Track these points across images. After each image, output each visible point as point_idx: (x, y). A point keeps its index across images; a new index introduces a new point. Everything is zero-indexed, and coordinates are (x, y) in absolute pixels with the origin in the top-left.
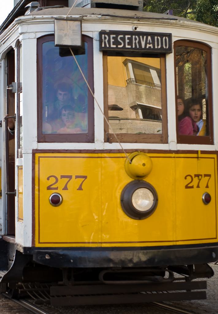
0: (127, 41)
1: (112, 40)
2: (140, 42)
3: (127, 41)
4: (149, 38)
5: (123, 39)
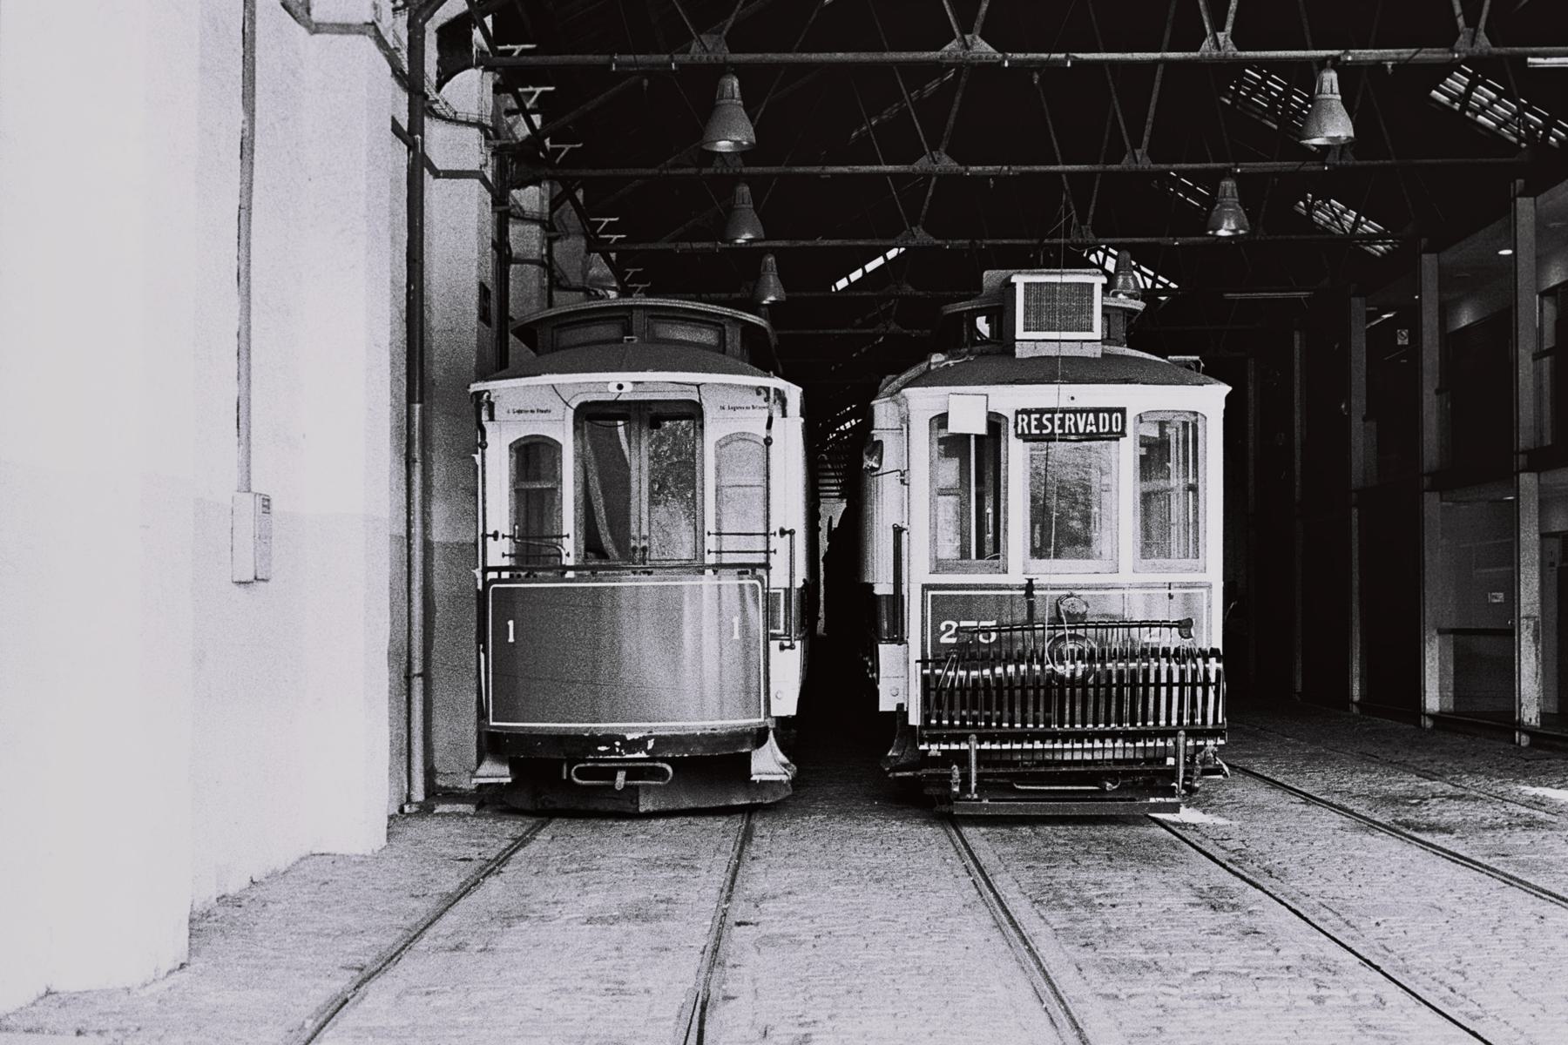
0: (1057, 422)
1: (1034, 423)
2: (1076, 424)
3: (1057, 422)
4: (1091, 416)
5: (1051, 420)
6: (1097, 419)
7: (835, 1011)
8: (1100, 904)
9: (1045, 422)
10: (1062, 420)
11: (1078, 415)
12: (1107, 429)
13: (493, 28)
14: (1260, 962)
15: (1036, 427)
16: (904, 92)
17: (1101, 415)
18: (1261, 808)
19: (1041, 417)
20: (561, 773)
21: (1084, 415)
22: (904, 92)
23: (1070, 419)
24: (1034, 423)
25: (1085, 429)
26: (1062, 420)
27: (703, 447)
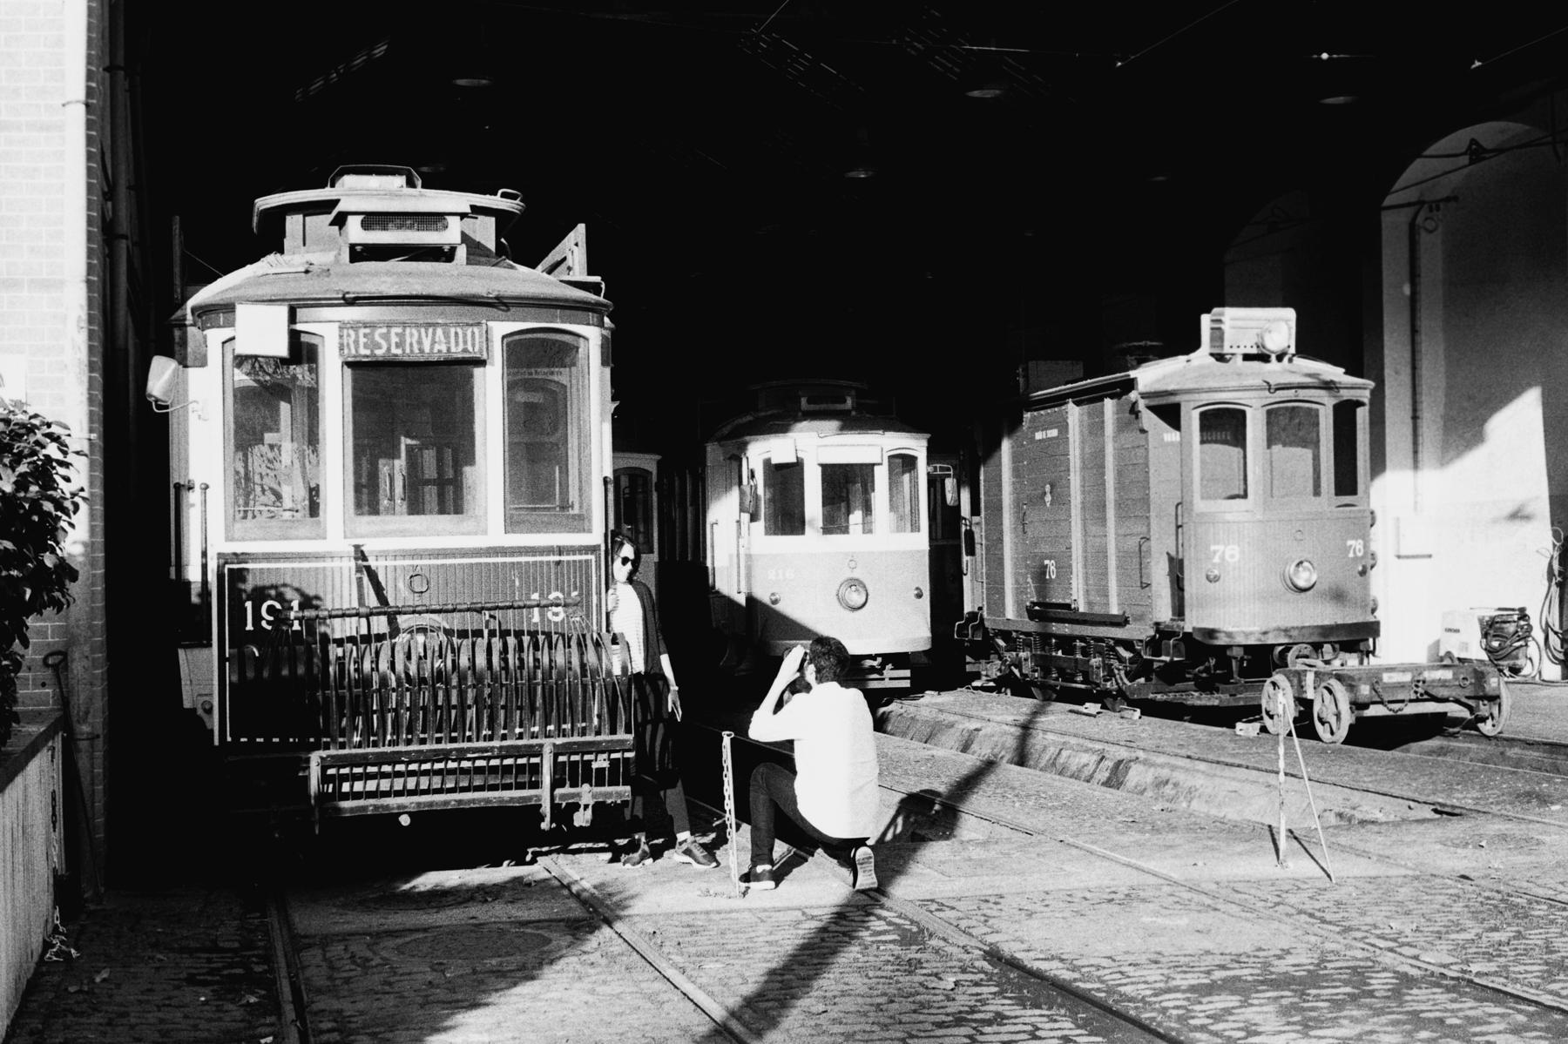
2: (420, 342)
3: (394, 339)
5: (386, 337)
6: (447, 336)
7: (1038, 907)
8: (1441, 974)
9: (377, 338)
10: (401, 336)
11: (423, 330)
12: (461, 347)
13: (656, 594)
14: (1344, 890)
15: (366, 346)
16: (178, 281)
17: (453, 330)
18: (1215, 775)
19: (372, 334)
20: (169, 573)
21: (431, 330)
22: (178, 281)
23: (412, 335)
24: (362, 340)
25: (432, 349)
26: (401, 336)
27: (486, 489)
